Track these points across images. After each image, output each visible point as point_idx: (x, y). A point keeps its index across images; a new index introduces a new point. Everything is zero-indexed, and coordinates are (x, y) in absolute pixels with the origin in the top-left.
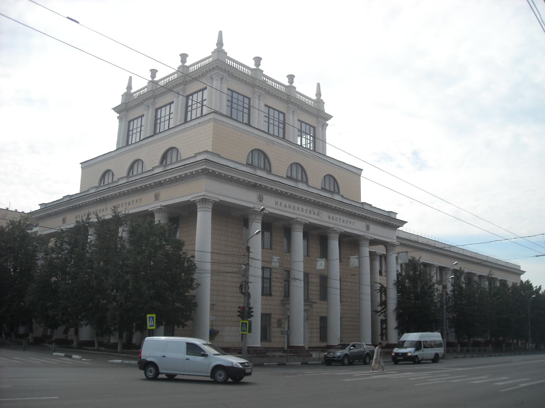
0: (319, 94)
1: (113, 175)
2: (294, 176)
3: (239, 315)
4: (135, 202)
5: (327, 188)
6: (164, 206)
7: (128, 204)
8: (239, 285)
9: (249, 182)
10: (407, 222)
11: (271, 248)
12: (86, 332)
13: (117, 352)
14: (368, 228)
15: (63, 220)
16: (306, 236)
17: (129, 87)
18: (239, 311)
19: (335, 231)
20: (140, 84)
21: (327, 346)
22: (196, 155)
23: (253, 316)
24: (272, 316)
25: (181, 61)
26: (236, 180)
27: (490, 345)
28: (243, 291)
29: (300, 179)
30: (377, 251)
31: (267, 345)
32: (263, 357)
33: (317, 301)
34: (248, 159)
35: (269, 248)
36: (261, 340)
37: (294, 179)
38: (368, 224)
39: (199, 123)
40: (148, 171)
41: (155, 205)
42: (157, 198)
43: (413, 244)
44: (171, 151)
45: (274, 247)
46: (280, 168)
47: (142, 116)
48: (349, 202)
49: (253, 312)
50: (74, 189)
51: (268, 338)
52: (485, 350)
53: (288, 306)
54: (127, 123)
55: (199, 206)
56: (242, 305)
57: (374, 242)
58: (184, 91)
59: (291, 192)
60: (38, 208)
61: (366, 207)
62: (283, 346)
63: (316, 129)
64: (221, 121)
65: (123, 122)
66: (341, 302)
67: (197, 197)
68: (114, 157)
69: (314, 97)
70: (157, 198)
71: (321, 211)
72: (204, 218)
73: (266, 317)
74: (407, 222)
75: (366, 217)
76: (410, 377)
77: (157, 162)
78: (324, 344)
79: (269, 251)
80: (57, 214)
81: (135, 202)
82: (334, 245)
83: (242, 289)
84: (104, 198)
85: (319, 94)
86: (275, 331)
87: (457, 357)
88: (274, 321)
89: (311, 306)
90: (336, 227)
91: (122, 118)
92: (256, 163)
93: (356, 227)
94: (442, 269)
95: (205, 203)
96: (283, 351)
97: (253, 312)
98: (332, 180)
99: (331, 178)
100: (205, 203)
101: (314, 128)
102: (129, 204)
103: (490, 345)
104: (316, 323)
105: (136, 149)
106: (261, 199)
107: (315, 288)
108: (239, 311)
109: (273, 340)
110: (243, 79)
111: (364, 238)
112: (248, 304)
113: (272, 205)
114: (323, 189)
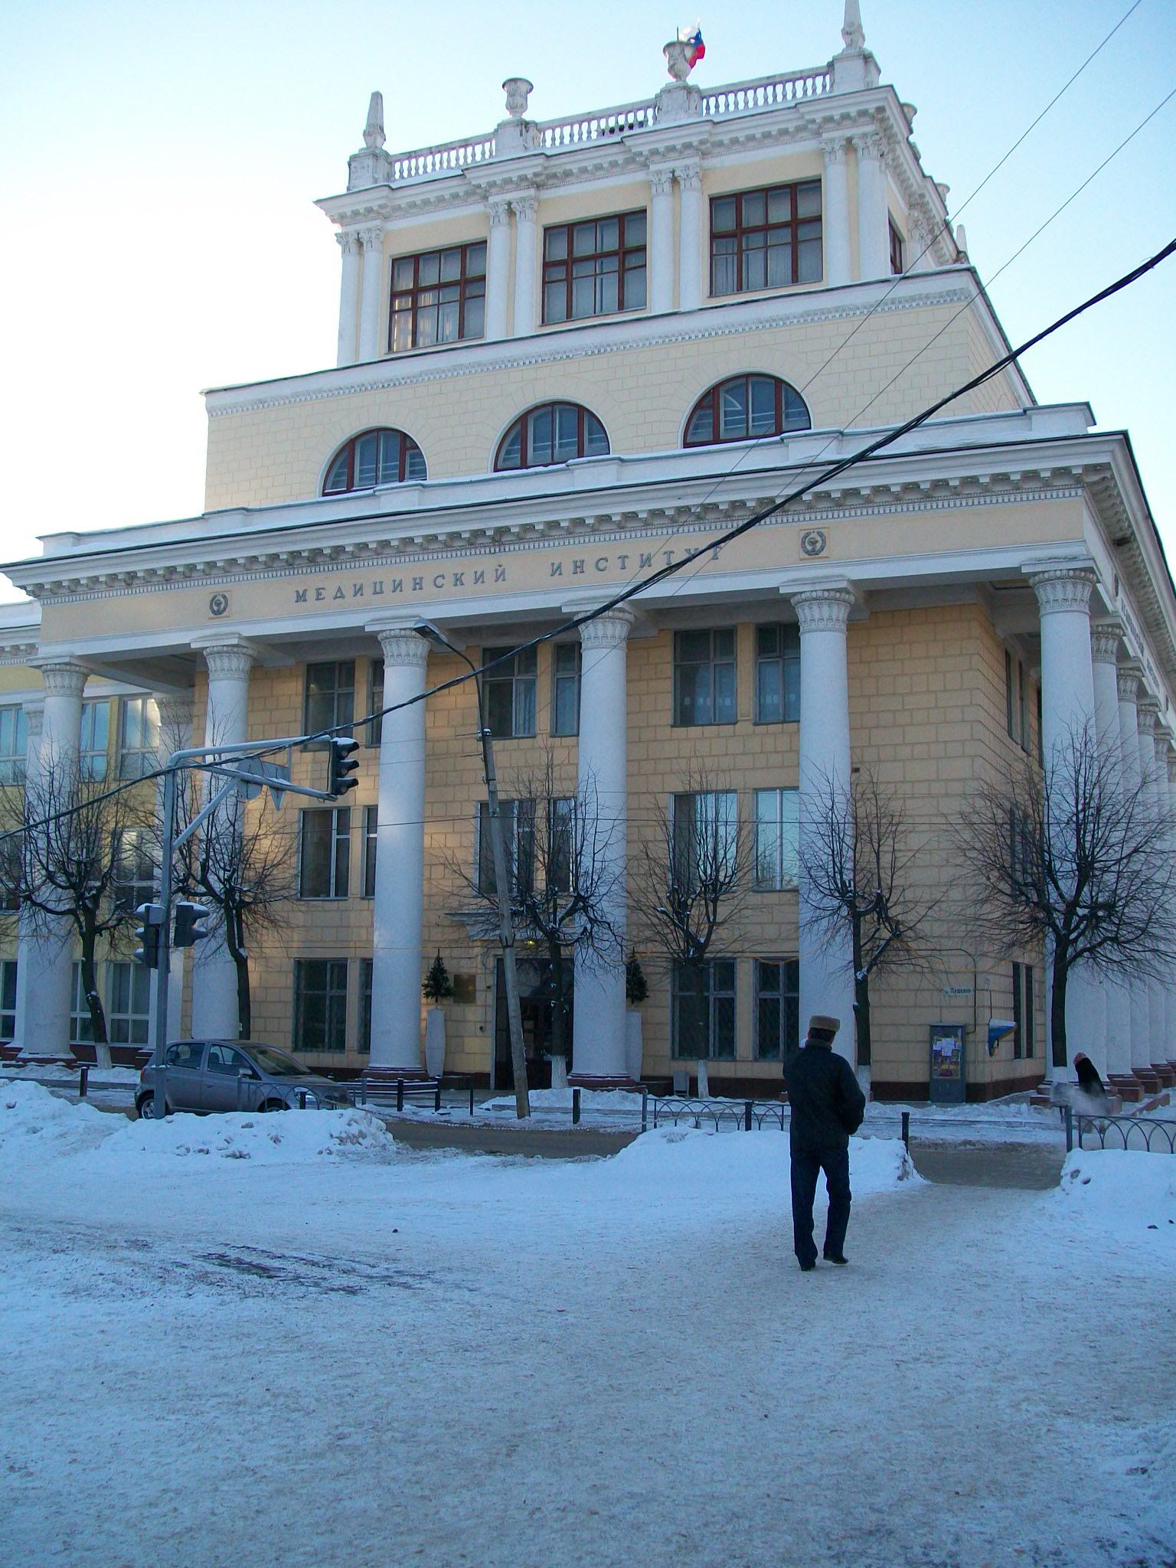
60: (37, 551)
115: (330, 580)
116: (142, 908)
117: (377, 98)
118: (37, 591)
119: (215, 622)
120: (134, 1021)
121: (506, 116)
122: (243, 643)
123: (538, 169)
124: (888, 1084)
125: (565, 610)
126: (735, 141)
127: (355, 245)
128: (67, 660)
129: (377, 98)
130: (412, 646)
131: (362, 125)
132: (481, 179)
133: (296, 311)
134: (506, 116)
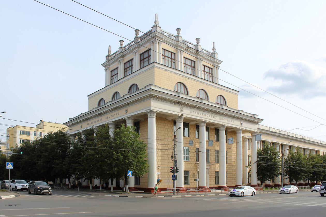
0: (214, 49)
1: (104, 101)
2: (201, 97)
3: (171, 172)
4: (116, 115)
5: (219, 103)
6: (131, 116)
7: (112, 116)
8: (171, 156)
9: (175, 101)
10: (263, 120)
11: (189, 137)
12: (97, 182)
13: (100, 191)
14: (241, 124)
15: (81, 126)
16: (207, 129)
17: (109, 52)
18: (171, 169)
19: (224, 126)
20: (115, 48)
21: (219, 186)
22: (146, 87)
23: (178, 172)
24: (190, 172)
25: (136, 34)
26: (168, 100)
27: (308, 185)
28: (173, 159)
29: (204, 98)
30: (279, 142)
31: (187, 186)
32: (202, 192)
33: (214, 163)
34: (175, 88)
35: (188, 136)
36: (184, 184)
37: (219, 104)
38: (242, 121)
39: (147, 69)
40: (122, 97)
41: (126, 116)
42: (127, 111)
43: (286, 137)
44: (133, 86)
45: (190, 136)
46: (213, 100)
47: (117, 68)
48: (248, 115)
49: (178, 169)
50: (86, 109)
51: (188, 184)
52: (305, 188)
53: (198, 167)
54: (110, 72)
55: (148, 115)
56: (172, 166)
57: (245, 131)
58: (138, 51)
59: (199, 105)
60: (68, 120)
61: (241, 112)
62: (196, 187)
63: (213, 70)
64: (159, 67)
65: (108, 72)
66: (226, 163)
67: (147, 110)
68: (104, 91)
69: (212, 51)
70: (127, 111)
71: (215, 115)
72: (153, 121)
73: (186, 172)
74: (263, 120)
75: (241, 118)
76: (258, 202)
77: (127, 92)
78: (217, 186)
79: (188, 138)
80: (77, 123)
81: (116, 115)
82: (223, 134)
83: (172, 158)
84: (100, 113)
85: (214, 49)
86: (191, 179)
87: (103, 192)
88: (191, 174)
89: (210, 166)
90: (224, 124)
91: (107, 70)
92: (179, 91)
93: (235, 124)
94: (282, 145)
95: (152, 113)
96: (196, 189)
97: (178, 169)
98: (204, 92)
99: (203, 91)
100: (152, 113)
101: (195, 62)
102: (113, 116)
103: (308, 185)
104: (214, 175)
105: (116, 85)
106: (241, 124)
107: (212, 157)
108: (171, 169)
109: (190, 184)
110: (182, 46)
111: (240, 130)
112: (176, 166)
113: (189, 113)
114: (217, 103)
115: (89, 122)
116: (72, 165)
117: (110, 46)
118: (69, 126)
119: (126, 114)
120: (9, 180)
121: (120, 46)
122: (112, 123)
123: (121, 55)
124: (140, 188)
125: (145, 112)
126: (127, 54)
127: (106, 70)
128: (128, 117)
129: (110, 46)
130: (131, 120)
131: (154, 21)
132: (131, 48)
133: (98, 80)
134: (154, 24)
